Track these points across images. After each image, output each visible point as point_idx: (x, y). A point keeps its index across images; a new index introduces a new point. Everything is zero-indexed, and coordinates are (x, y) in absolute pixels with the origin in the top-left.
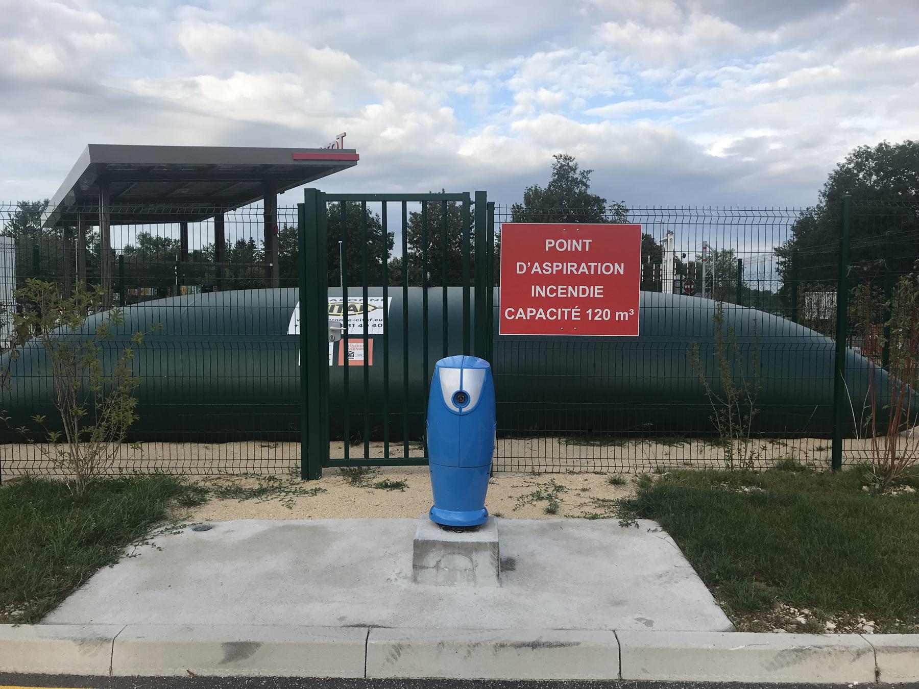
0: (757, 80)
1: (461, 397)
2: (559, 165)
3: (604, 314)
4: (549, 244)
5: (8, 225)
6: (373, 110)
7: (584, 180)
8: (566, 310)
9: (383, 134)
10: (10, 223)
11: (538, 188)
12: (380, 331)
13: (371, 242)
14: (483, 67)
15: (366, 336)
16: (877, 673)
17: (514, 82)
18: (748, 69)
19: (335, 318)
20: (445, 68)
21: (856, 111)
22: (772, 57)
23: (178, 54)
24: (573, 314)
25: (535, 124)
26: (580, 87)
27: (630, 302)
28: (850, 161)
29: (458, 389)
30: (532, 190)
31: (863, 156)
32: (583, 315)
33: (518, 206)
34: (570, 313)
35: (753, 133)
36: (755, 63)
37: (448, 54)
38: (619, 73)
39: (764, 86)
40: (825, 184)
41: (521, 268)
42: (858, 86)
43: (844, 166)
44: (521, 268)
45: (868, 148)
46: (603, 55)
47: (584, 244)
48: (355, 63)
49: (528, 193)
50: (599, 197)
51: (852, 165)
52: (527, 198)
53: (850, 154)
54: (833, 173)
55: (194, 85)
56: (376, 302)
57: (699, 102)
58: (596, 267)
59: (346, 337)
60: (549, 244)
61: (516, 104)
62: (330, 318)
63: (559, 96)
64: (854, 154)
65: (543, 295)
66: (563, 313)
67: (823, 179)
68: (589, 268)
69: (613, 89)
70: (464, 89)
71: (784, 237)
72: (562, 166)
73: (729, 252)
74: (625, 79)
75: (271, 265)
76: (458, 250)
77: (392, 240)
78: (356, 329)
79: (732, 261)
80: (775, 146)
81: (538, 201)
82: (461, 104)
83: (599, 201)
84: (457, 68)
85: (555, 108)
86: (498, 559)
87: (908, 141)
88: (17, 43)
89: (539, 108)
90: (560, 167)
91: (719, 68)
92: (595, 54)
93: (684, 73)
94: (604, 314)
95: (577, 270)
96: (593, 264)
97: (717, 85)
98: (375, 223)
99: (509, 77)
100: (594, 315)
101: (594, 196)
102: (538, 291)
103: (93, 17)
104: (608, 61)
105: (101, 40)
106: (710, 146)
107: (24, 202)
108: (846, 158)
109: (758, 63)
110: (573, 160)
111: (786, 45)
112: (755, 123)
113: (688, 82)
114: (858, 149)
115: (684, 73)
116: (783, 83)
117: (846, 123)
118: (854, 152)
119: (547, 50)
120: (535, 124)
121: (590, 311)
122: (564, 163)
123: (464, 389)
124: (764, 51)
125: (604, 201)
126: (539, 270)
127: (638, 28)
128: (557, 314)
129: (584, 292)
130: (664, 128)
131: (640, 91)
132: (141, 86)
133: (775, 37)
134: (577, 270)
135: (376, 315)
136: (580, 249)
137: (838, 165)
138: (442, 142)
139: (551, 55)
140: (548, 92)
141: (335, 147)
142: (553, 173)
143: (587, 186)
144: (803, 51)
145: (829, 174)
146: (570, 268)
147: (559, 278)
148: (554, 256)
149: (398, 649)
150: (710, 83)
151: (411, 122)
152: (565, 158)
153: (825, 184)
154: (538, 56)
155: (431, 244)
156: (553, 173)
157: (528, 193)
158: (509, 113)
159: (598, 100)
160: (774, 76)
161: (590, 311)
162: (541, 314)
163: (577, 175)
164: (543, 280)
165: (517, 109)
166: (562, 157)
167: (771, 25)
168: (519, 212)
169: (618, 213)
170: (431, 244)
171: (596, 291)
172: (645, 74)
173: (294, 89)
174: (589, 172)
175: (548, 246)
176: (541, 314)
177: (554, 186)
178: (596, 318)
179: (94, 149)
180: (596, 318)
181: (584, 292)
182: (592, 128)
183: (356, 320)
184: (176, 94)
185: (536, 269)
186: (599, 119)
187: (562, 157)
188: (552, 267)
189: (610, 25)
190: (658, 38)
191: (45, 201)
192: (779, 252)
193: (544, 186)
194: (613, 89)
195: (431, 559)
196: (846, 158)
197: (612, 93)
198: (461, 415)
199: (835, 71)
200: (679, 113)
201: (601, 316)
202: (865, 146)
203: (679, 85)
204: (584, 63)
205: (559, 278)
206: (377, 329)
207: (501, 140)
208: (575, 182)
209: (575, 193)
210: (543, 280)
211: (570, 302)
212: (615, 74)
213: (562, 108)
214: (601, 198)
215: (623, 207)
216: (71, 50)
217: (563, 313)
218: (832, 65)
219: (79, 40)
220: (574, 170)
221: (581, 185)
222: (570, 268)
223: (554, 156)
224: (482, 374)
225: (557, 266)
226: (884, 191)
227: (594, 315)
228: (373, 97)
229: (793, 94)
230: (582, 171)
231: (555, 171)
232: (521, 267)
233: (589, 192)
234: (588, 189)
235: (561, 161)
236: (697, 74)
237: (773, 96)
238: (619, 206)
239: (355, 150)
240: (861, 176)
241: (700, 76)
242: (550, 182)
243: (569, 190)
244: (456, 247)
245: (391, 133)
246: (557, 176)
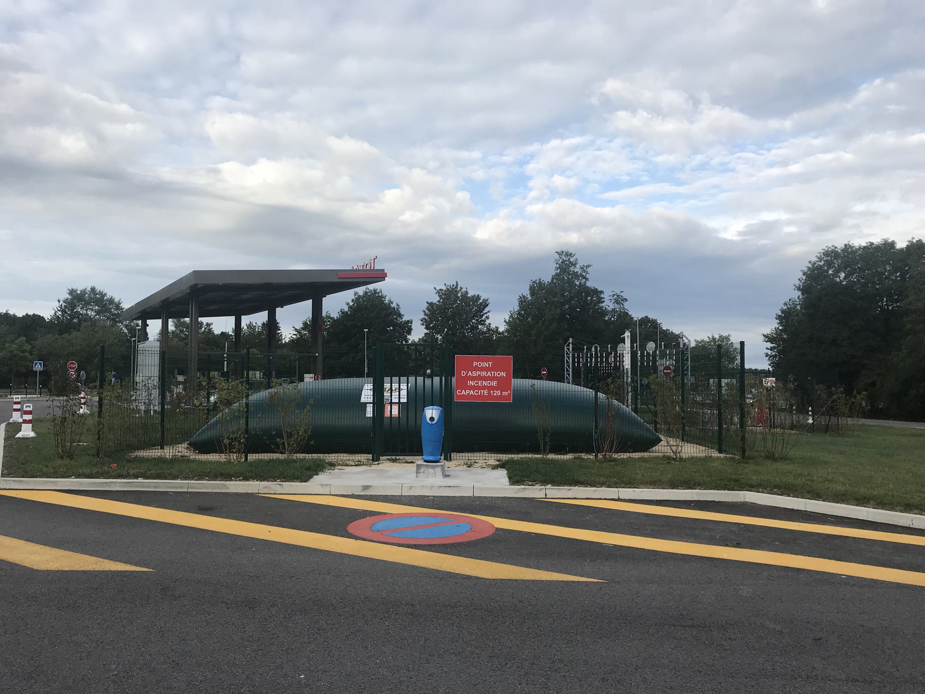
0: (772, 165)
1: (432, 419)
2: (561, 260)
3: (498, 393)
4: (475, 364)
5: (57, 310)
6: (391, 196)
7: (584, 274)
8: (482, 391)
9: (402, 218)
10: (59, 309)
11: (541, 281)
12: (405, 401)
13: (391, 328)
14: (501, 154)
15: (399, 403)
16: (546, 495)
17: (531, 167)
18: (762, 154)
19: (387, 394)
20: (464, 154)
21: (867, 195)
22: (785, 144)
23: (205, 140)
24: (485, 393)
25: (550, 208)
26: (594, 172)
27: (508, 388)
28: (820, 259)
30: (536, 283)
31: (831, 255)
32: (489, 393)
33: (524, 296)
34: (484, 392)
35: (768, 216)
36: (769, 150)
37: (467, 141)
38: (634, 158)
39: (776, 171)
40: (799, 279)
41: (463, 373)
42: (871, 171)
43: (815, 263)
44: (463, 373)
45: (836, 248)
46: (618, 142)
48: (374, 150)
49: (533, 285)
50: (597, 289)
51: (823, 262)
52: (533, 290)
53: (820, 253)
54: (806, 269)
55: (217, 171)
56: (404, 386)
57: (715, 186)
58: (494, 373)
59: (391, 403)
60: (475, 364)
61: (531, 189)
62: (385, 394)
63: (573, 182)
64: (823, 253)
65: (473, 384)
67: (797, 277)
68: (491, 374)
69: (629, 174)
70: (479, 174)
71: (771, 326)
72: (564, 261)
73: (726, 338)
74: (641, 164)
75: (317, 355)
76: (470, 335)
77: (411, 326)
78: (395, 400)
79: (729, 346)
80: (792, 229)
81: (542, 292)
82: (478, 190)
83: (597, 292)
84: (476, 154)
85: (569, 193)
87: (870, 242)
88: (49, 132)
89: (554, 193)
90: (562, 262)
91: (733, 154)
92: (610, 141)
93: (699, 158)
94: (498, 393)
95: (486, 374)
96: (493, 372)
97: (732, 170)
98: (395, 312)
99: (527, 163)
100: (494, 393)
101: (593, 288)
102: (471, 383)
103: (124, 108)
104: (623, 148)
105: (132, 129)
106: (725, 229)
107: (73, 289)
108: (816, 256)
109: (771, 149)
110: (574, 256)
111: (803, 130)
112: (769, 207)
113: (703, 167)
114: (826, 249)
115: (699, 158)
116: (795, 168)
117: (859, 207)
118: (823, 251)
119: (562, 137)
120: (550, 208)
122: (565, 259)
123: (433, 416)
124: (776, 138)
125: (602, 292)
126: (471, 374)
127: (650, 116)
128: (478, 393)
129: (489, 383)
130: (679, 212)
131: (655, 174)
132: (167, 173)
133: (788, 124)
134: (486, 374)
135: (404, 393)
136: (487, 366)
137: (810, 263)
138: (459, 225)
139: (568, 142)
140: (562, 178)
141: (368, 268)
142: (556, 267)
143: (587, 279)
144: (816, 138)
145: (801, 271)
146: (484, 374)
147: (479, 378)
148: (477, 369)
149: (411, 487)
150: (724, 169)
151: (429, 207)
152: (566, 254)
153: (799, 279)
154: (555, 143)
155: (446, 330)
156: (556, 267)
157: (533, 285)
158: (524, 198)
159: (614, 184)
160: (785, 162)
162: (472, 392)
163: (577, 269)
164: (473, 379)
165: (533, 194)
166: (564, 253)
167: (784, 113)
168: (525, 301)
169: (617, 302)
170: (446, 330)
171: (494, 383)
172: (660, 159)
173: (315, 174)
174: (588, 266)
176: (472, 392)
177: (556, 279)
178: (495, 394)
180: (495, 394)
181: (489, 383)
182: (607, 212)
183: (395, 394)
184: (200, 180)
185: (470, 373)
186: (613, 203)
187: (564, 253)
188: (476, 373)
189: (621, 114)
190: (670, 126)
191: (91, 289)
192: (769, 338)
193: (547, 279)
194: (629, 174)
195: (422, 470)
196: (816, 256)
197: (627, 178)
198: (432, 424)
199: (848, 157)
200: (694, 196)
201: (497, 394)
202: (833, 246)
203: (693, 170)
204: (599, 149)
205: (479, 378)
206: (404, 400)
207: (518, 223)
208: (576, 276)
209: (576, 285)
210: (473, 379)
211: (484, 388)
212: (631, 159)
213: (577, 193)
214: (599, 290)
215: (622, 296)
216: (101, 138)
218: (845, 151)
219: (111, 129)
220: (575, 265)
221: (581, 278)
222: (484, 374)
223: (557, 252)
224: (439, 411)
225: (478, 373)
226: (851, 285)
227: (494, 393)
228: (390, 182)
229: (806, 178)
230: (582, 266)
231: (558, 266)
232: (464, 373)
233: (588, 284)
234: (588, 282)
235: (563, 257)
236: (712, 159)
237: (787, 180)
238: (618, 296)
239: (384, 270)
240: (830, 272)
241: (714, 162)
242: (553, 276)
243: (571, 283)
244: (468, 333)
245: (407, 216)
246: (559, 270)
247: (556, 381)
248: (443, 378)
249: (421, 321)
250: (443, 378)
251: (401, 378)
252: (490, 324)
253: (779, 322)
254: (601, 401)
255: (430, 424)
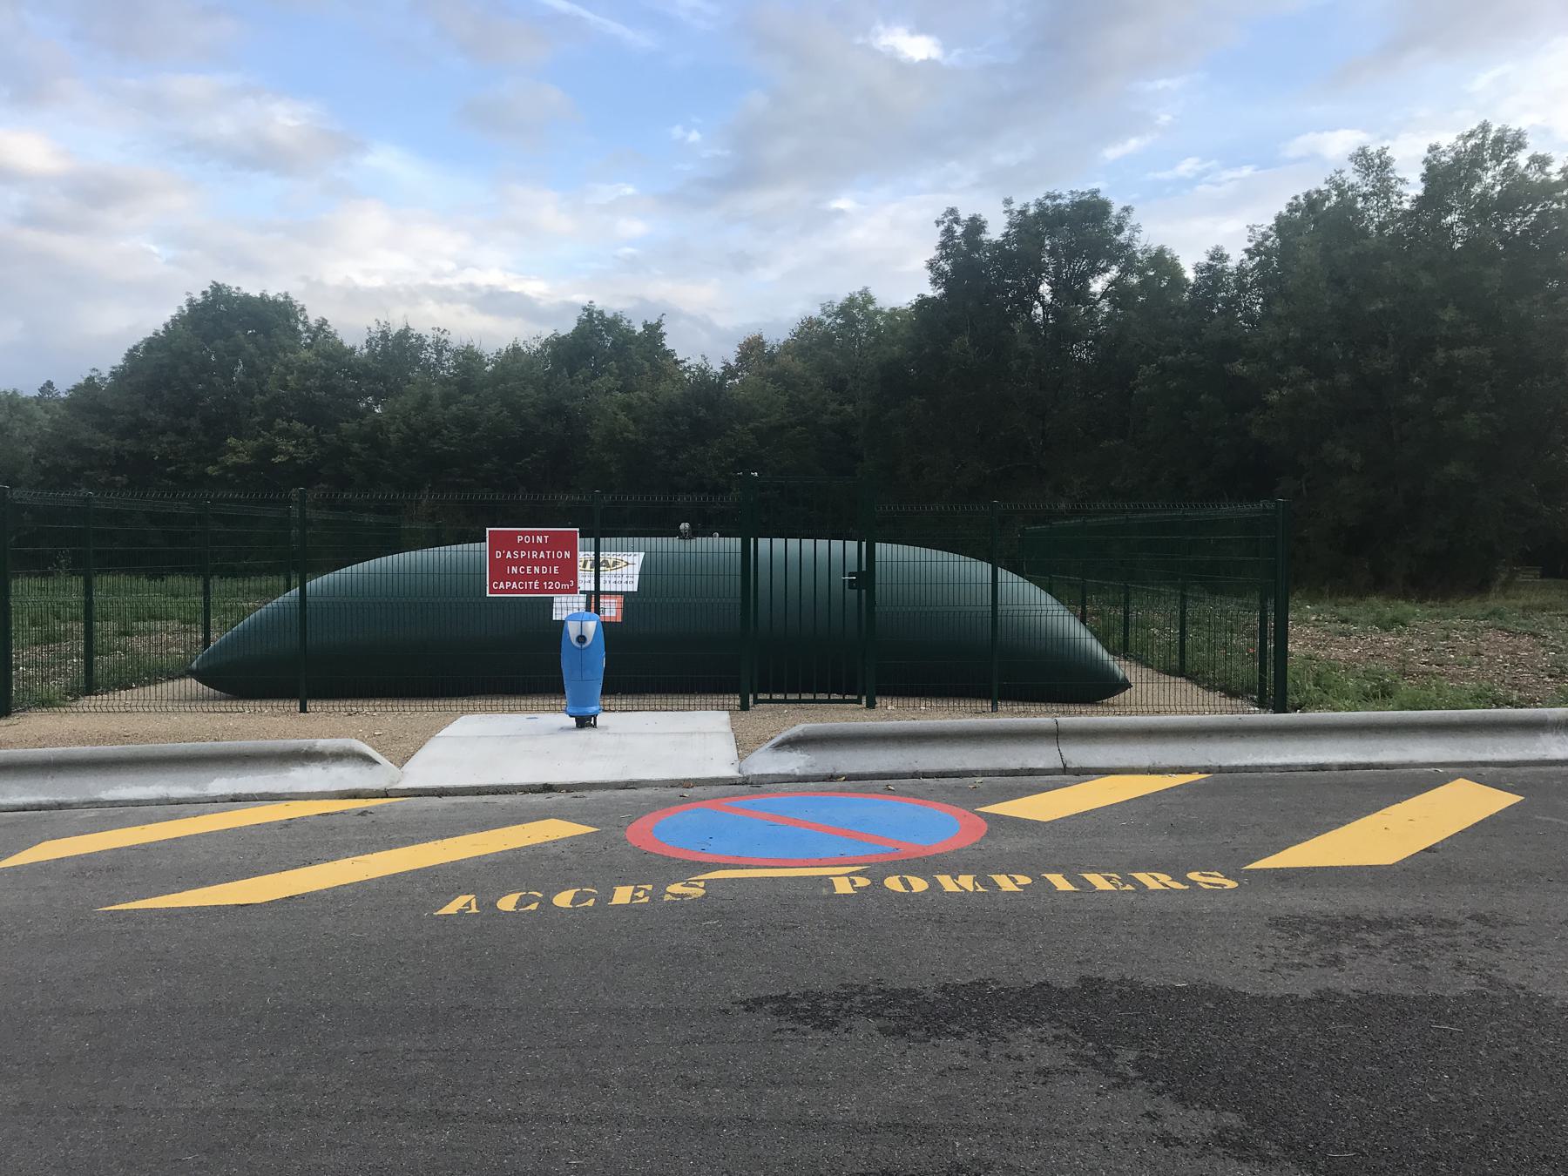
8: (531, 583)
29: (579, 634)
34: (533, 585)
47: (544, 539)
58: (551, 554)
66: (528, 585)
86: (573, 729)
96: (548, 552)
100: (548, 586)
121: (545, 583)
123: (583, 634)
161: (545, 583)
164: (513, 562)
175: (519, 540)
178: (550, 588)
179: (217, 288)
180: (550, 588)
188: (519, 554)
210: (513, 562)
217: (528, 585)
227: (548, 586)
247: (894, 543)
248: (864, 544)
249: (919, 296)
250: (864, 544)
251: (818, 540)
252: (1326, 182)
253: (1232, 264)
254: (1005, 608)
255: (578, 649)
